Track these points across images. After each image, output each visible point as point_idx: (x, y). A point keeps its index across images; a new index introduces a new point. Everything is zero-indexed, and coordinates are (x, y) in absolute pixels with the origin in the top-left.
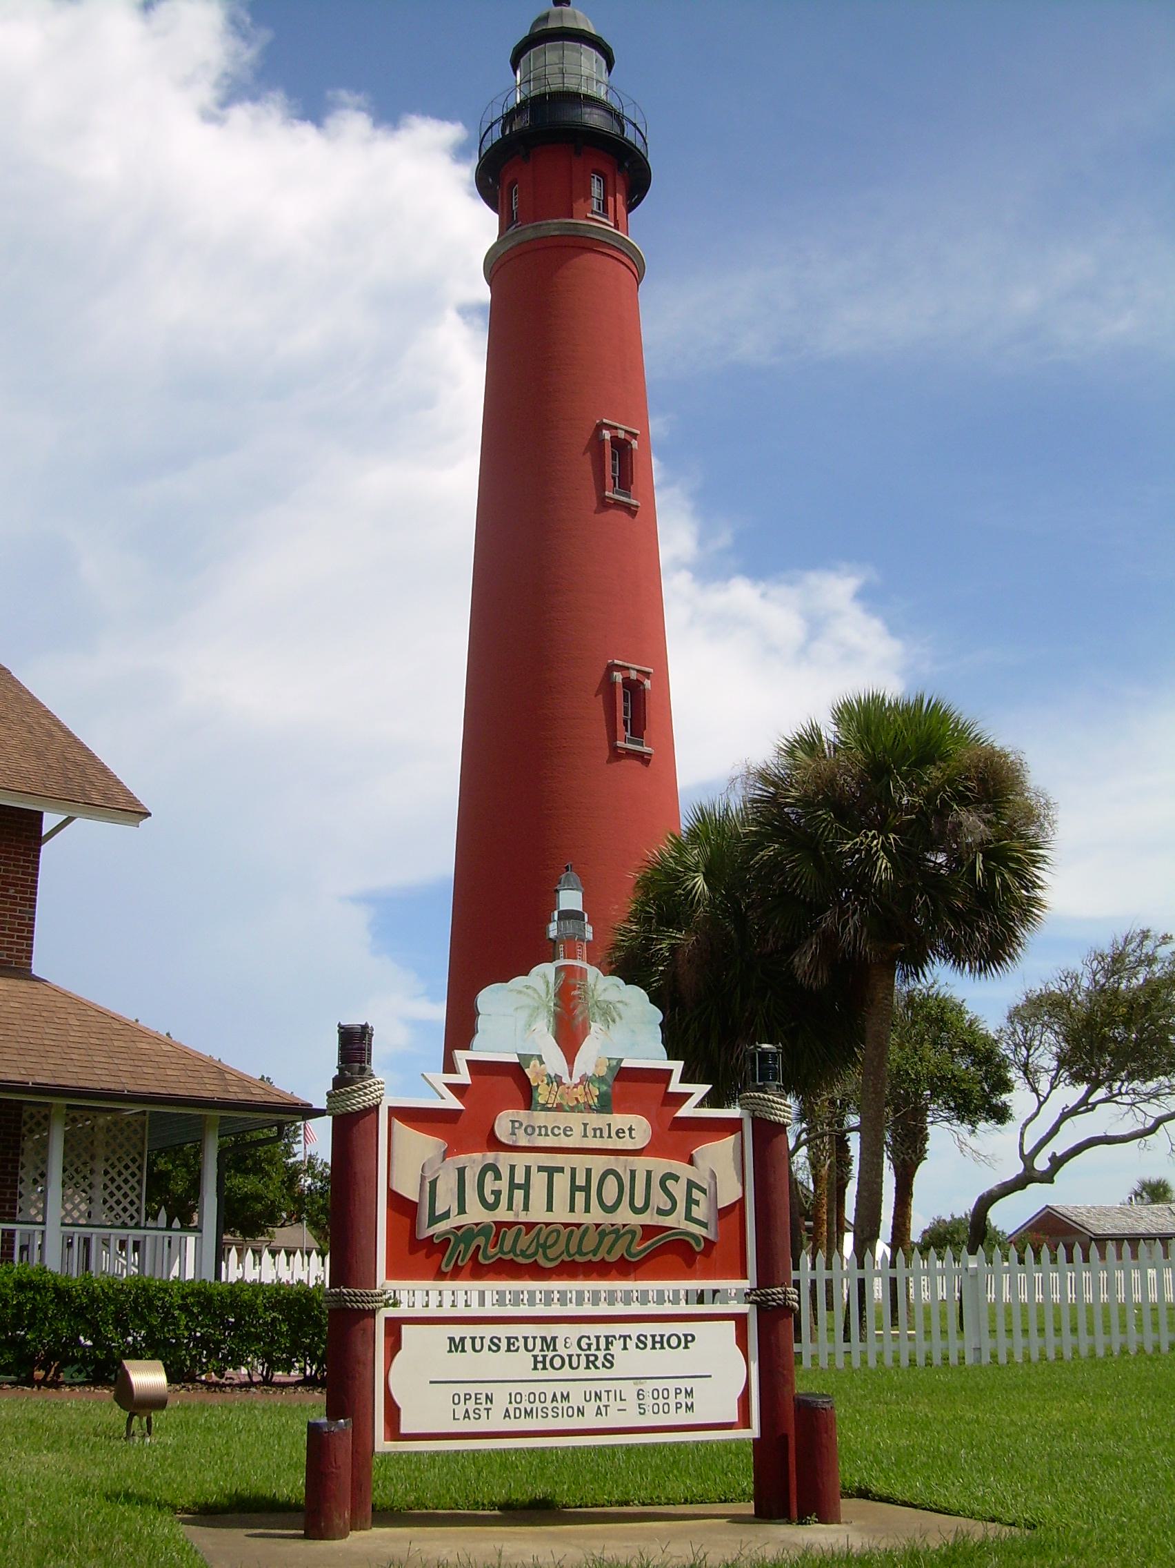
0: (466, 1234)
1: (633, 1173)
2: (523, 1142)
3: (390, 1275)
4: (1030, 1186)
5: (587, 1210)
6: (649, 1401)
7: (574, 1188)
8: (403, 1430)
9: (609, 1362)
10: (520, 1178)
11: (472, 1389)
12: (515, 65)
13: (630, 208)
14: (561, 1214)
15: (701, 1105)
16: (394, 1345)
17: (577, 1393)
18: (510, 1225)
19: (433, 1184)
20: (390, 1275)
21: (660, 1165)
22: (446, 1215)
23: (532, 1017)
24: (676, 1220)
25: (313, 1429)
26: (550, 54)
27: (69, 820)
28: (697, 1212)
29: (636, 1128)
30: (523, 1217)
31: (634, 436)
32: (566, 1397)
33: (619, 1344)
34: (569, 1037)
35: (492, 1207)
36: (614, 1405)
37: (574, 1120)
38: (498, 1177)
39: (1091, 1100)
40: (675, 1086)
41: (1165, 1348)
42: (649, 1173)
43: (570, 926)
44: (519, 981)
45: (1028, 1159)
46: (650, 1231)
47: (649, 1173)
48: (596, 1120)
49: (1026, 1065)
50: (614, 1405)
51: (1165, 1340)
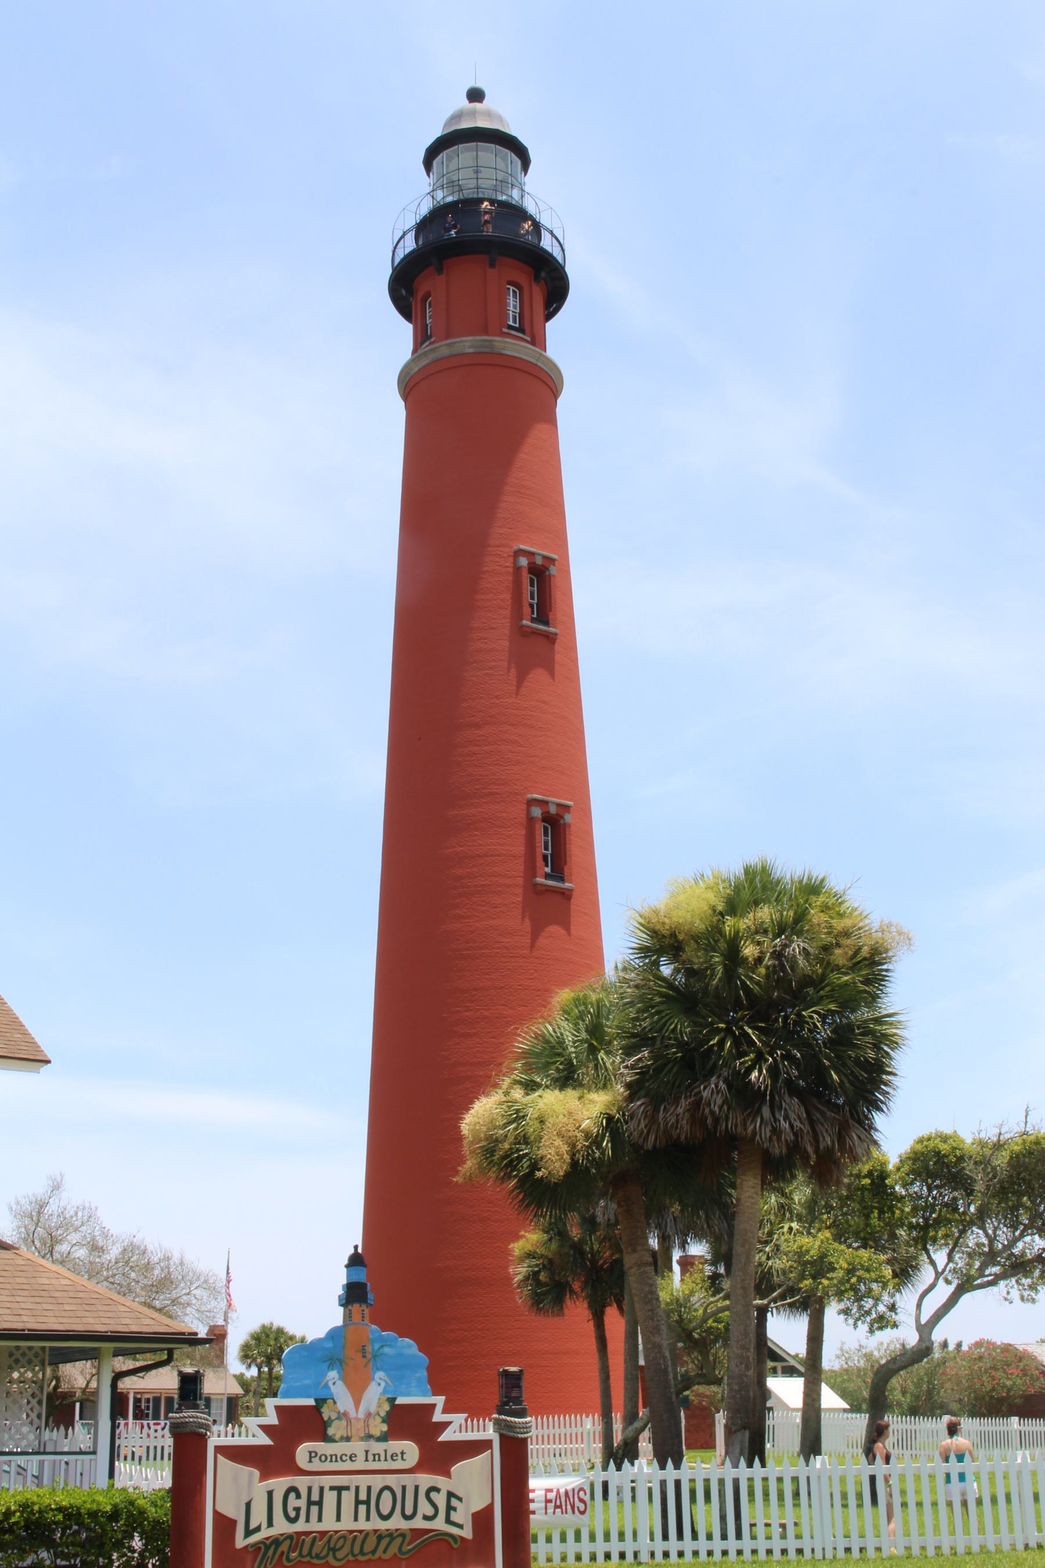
2: (317, 1466)
5: (368, 1518)
7: (358, 1502)
10: (315, 1497)
12: (428, 164)
13: (549, 316)
14: (347, 1524)
21: (425, 1480)
22: (258, 1529)
24: (439, 1524)
28: (455, 1517)
29: (410, 1450)
37: (357, 1447)
40: (438, 1417)
47: (417, 1488)
48: (378, 1447)
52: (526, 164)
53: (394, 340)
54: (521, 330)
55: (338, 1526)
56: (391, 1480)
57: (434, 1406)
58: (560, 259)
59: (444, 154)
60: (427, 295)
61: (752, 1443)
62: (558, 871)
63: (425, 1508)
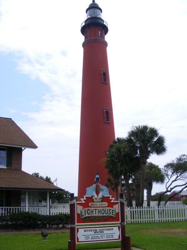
0: (86, 218)
1: (106, 210)
2: (92, 206)
3: (77, 223)
5: (100, 214)
6: (108, 237)
7: (99, 212)
8: (79, 241)
9: (103, 232)
10: (92, 211)
11: (87, 236)
12: (86, 12)
14: (97, 215)
15: (114, 201)
17: (99, 236)
19: (82, 212)
21: (109, 208)
22: (83, 216)
24: (111, 215)
28: (113, 214)
29: (106, 204)
30: (93, 215)
31: (106, 72)
32: (98, 236)
34: (98, 193)
35: (89, 214)
36: (104, 237)
37: (98, 203)
38: (89, 211)
39: (177, 179)
40: (111, 198)
42: (107, 209)
45: (167, 189)
47: (107, 209)
48: (101, 203)
52: (101, 12)
53: (82, 38)
54: (101, 37)
58: (107, 26)
59: (90, 10)
60: (87, 31)
61: (140, 204)
62: (108, 120)
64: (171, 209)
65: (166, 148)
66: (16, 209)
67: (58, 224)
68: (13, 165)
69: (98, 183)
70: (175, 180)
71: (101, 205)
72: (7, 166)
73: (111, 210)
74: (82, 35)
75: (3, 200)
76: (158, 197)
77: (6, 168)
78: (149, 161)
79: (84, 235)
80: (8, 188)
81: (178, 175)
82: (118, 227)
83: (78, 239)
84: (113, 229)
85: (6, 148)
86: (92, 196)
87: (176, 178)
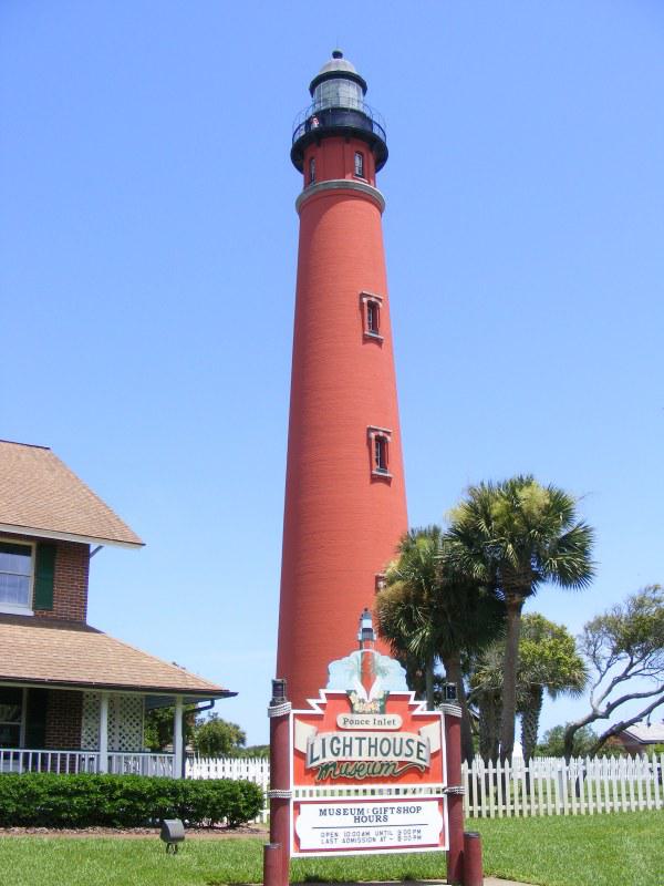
0: (326, 767)
1: (395, 739)
2: (349, 727)
4: (597, 720)
5: (376, 755)
6: (402, 835)
7: (370, 746)
9: (386, 819)
10: (348, 743)
11: (330, 831)
12: (312, 90)
13: (377, 170)
14: (365, 757)
16: (442, 835)
17: (373, 831)
18: (344, 762)
19: (312, 745)
20: (297, 782)
21: (406, 735)
22: (318, 759)
23: (351, 676)
24: (413, 759)
25: (266, 848)
26: (326, 88)
27: (100, 547)
28: (422, 755)
29: (396, 720)
30: (349, 759)
33: (390, 811)
34: (367, 680)
35: (336, 755)
36: (388, 837)
37: (370, 717)
38: (339, 742)
39: (629, 673)
40: (412, 702)
41: (658, 807)
43: (367, 634)
44: (346, 659)
46: (402, 763)
48: (379, 717)
49: (594, 656)
50: (388, 837)
51: (659, 803)
55: (359, 759)
56: (389, 736)
57: (409, 696)
63: (406, 750)
64: (614, 778)
65: (592, 566)
66: (63, 756)
67: (216, 818)
68: (57, 606)
69: (368, 648)
70: (625, 676)
71: (380, 722)
72: (34, 608)
73: (412, 741)
74: (299, 173)
75: (18, 727)
76: (561, 744)
77: (31, 613)
78: (530, 607)
79: (320, 827)
80: (41, 682)
81: (635, 660)
82: (436, 803)
83: (297, 840)
84: (419, 809)
85: (33, 544)
86: (349, 692)
87: (628, 670)
